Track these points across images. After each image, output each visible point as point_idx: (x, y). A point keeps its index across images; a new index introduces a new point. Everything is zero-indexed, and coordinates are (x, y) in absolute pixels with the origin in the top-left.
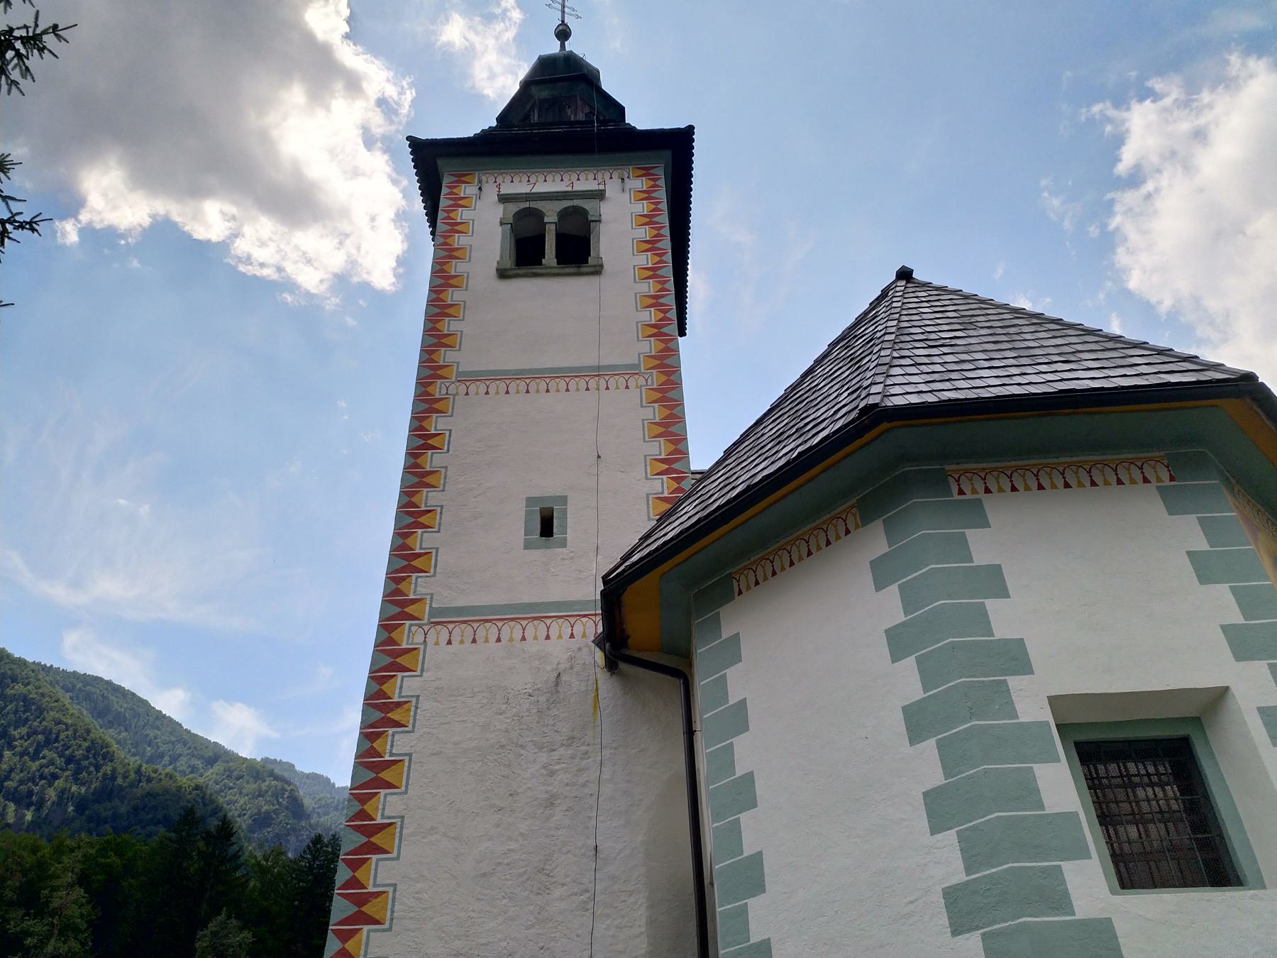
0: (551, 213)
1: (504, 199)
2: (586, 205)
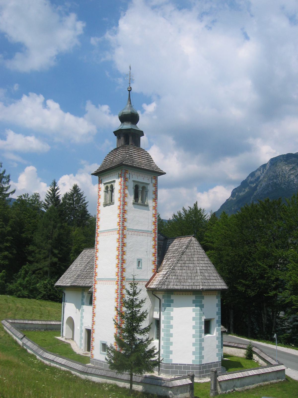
0: (141, 186)
1: (134, 181)
2: (146, 186)
